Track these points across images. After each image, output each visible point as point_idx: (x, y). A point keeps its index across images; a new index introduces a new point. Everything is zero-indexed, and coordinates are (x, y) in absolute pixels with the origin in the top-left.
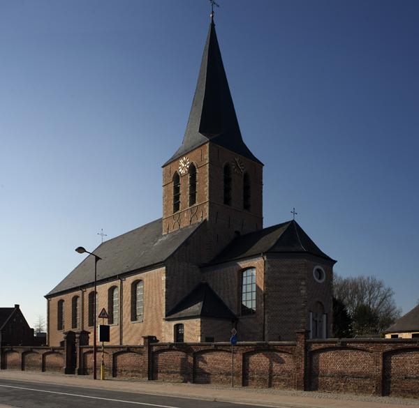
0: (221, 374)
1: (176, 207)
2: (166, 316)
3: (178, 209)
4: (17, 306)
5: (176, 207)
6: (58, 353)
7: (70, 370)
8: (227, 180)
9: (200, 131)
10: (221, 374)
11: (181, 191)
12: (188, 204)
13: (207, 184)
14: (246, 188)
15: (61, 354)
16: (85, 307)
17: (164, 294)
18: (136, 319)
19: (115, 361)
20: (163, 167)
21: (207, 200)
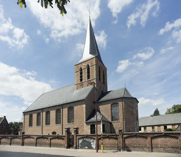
0: (169, 147)
1: (81, 80)
2: (86, 121)
3: (89, 78)
4: (5, 117)
5: (81, 80)
6: (8, 138)
7: (69, 146)
8: (100, 72)
9: (90, 54)
10: (169, 147)
11: (83, 74)
12: (87, 79)
13: (95, 72)
14: (104, 76)
15: (9, 138)
16: (43, 117)
17: (85, 112)
18: (49, 124)
19: (50, 142)
20: (75, 65)
21: (95, 78)
